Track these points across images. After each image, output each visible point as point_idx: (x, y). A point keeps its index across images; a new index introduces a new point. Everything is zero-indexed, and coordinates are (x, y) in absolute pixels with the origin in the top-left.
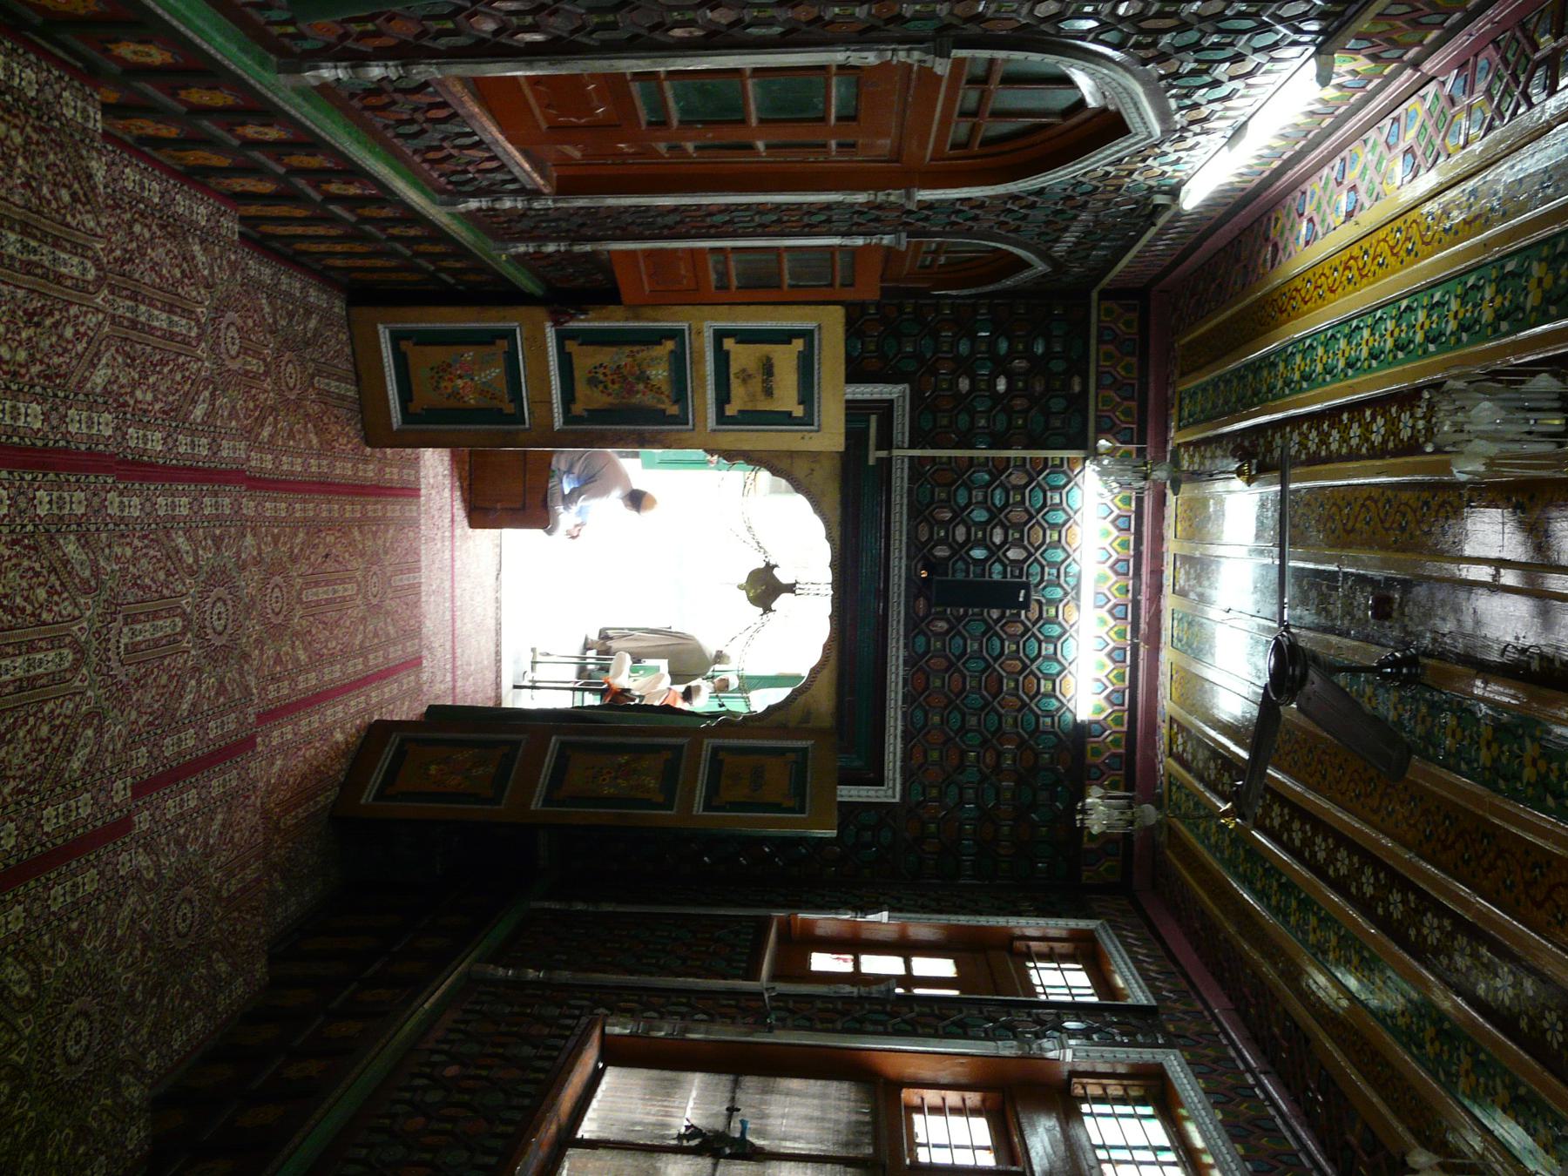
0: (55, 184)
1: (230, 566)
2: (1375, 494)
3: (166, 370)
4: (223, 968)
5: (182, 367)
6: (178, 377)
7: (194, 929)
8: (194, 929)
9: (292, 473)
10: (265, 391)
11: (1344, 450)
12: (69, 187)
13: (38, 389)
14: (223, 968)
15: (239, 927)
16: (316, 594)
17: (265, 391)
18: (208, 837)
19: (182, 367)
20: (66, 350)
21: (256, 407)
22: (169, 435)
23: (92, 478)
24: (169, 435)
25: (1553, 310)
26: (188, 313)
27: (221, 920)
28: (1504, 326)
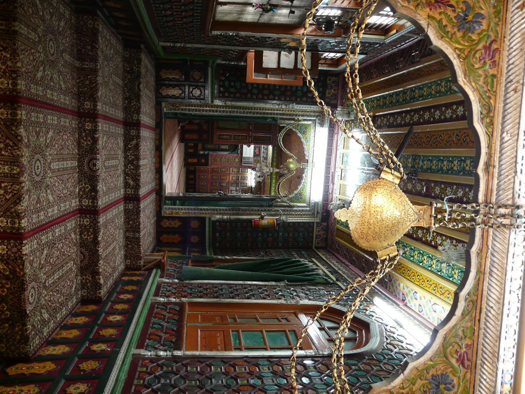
0: (28, 7)
1: (42, 145)
2: (398, 136)
3: (26, 54)
4: (46, 316)
5: (32, 54)
6: (31, 58)
7: (36, 301)
8: (36, 301)
9: (65, 104)
10: (39, 52)
11: (403, 122)
12: (32, 8)
13: (24, 76)
14: (46, 316)
15: (52, 299)
16: (72, 164)
17: (39, 52)
18: (40, 260)
19: (32, 54)
20: (31, 64)
21: (34, 60)
22: (45, 89)
23: (28, 106)
24: (45, 89)
25: (421, 86)
26: (35, 30)
27: (46, 296)
28: (414, 89)
